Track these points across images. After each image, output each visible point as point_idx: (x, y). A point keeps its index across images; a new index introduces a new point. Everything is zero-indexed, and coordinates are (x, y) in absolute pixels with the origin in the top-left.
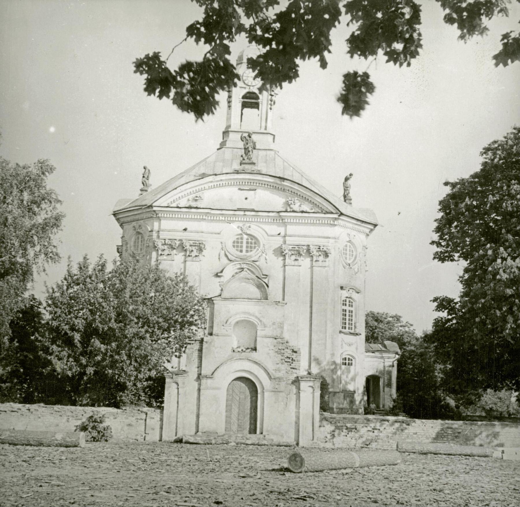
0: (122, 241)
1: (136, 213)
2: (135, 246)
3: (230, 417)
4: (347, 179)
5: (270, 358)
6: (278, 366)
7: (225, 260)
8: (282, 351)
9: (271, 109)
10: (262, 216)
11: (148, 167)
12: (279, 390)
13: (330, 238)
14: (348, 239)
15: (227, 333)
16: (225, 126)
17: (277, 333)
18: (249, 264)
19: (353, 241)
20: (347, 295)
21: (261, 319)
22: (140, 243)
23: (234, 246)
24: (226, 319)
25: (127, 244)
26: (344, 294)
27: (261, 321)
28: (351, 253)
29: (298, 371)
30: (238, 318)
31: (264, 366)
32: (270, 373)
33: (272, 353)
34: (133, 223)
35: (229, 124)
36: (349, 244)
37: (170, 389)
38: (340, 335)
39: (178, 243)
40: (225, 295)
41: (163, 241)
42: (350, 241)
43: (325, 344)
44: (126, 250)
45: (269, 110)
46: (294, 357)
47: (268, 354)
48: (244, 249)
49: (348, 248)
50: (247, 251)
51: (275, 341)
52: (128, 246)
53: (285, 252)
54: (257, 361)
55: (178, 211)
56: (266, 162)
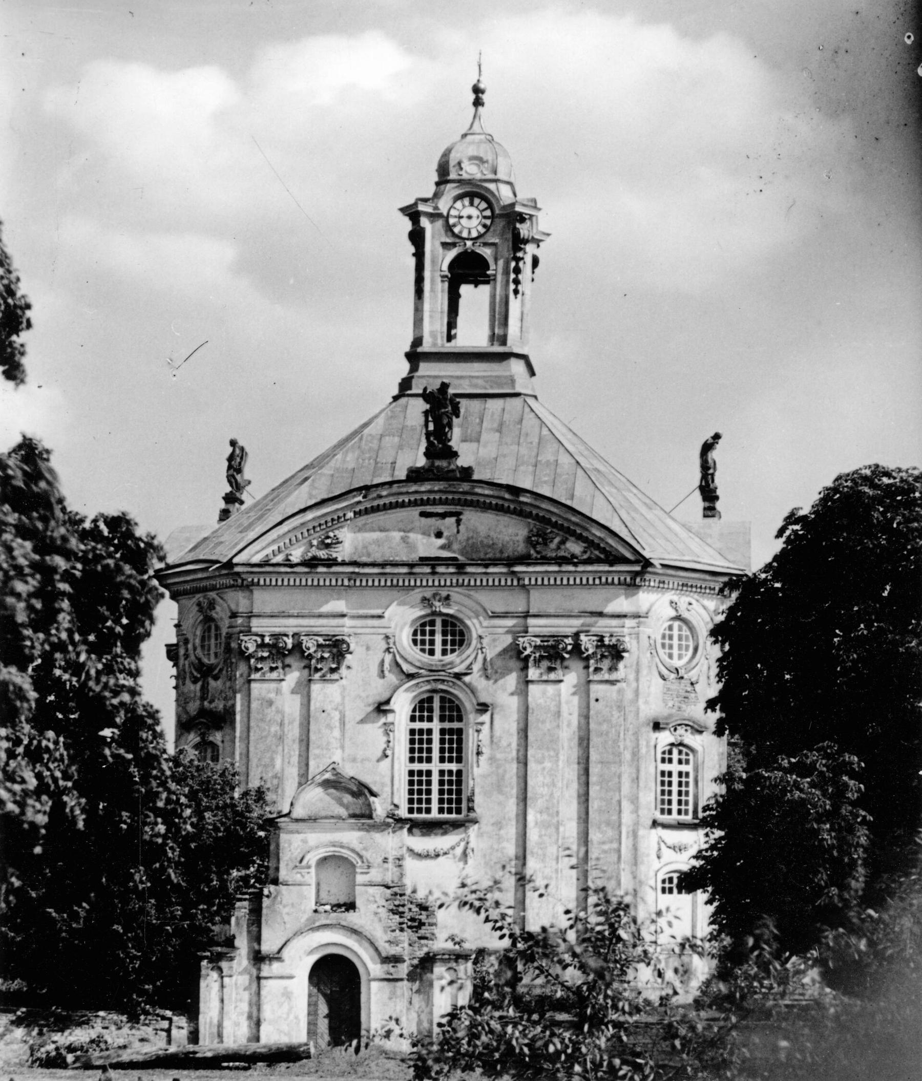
0: (178, 636)
1: (200, 576)
2: (203, 647)
3: (315, 1025)
4: (707, 448)
5: (380, 920)
6: (394, 934)
7: (392, 678)
8: (401, 909)
9: (516, 292)
10: (474, 573)
11: (241, 443)
12: (395, 976)
13: (625, 616)
14: (673, 613)
15: (302, 880)
16: (410, 339)
17: (389, 876)
18: (448, 681)
19: (685, 615)
20: (672, 739)
21: (363, 853)
22: (213, 641)
23: (415, 642)
24: (301, 856)
25: (186, 641)
26: (665, 738)
27: (361, 857)
28: (684, 643)
29: (431, 942)
30: (322, 853)
31: (369, 936)
32: (380, 949)
33: (383, 912)
34: (198, 596)
35: (419, 335)
36: (676, 624)
37: (209, 978)
38: (653, 831)
39: (290, 642)
40: (295, 815)
41: (259, 640)
42: (678, 618)
43: (619, 851)
44: (186, 656)
45: (512, 295)
46: (423, 917)
47: (376, 913)
48: (438, 647)
49: (675, 633)
50: (444, 652)
51: (389, 892)
52: (190, 646)
53: (526, 653)
54: (355, 927)
55: (287, 573)
56: (499, 430)
